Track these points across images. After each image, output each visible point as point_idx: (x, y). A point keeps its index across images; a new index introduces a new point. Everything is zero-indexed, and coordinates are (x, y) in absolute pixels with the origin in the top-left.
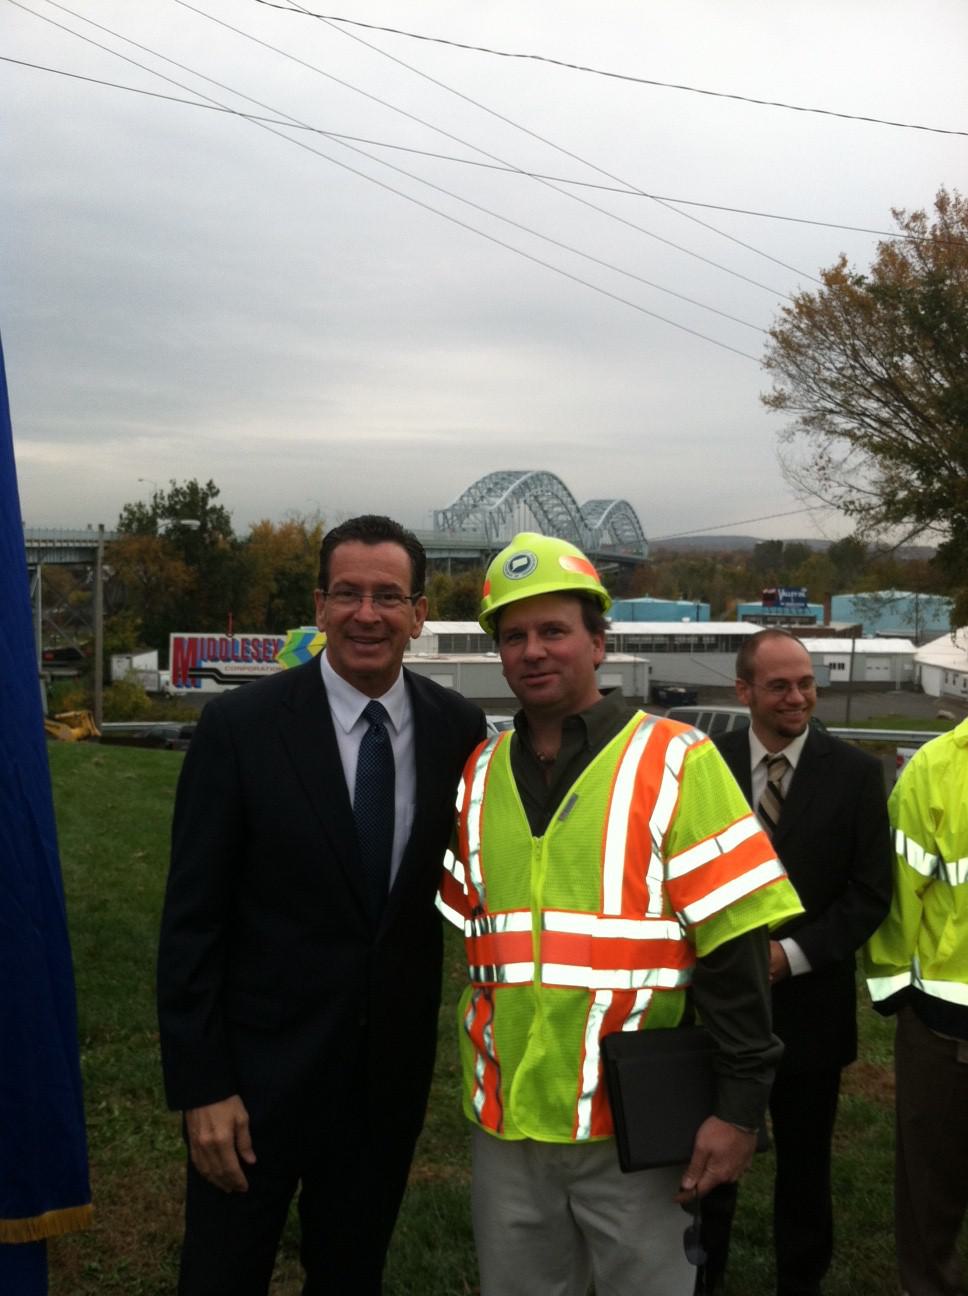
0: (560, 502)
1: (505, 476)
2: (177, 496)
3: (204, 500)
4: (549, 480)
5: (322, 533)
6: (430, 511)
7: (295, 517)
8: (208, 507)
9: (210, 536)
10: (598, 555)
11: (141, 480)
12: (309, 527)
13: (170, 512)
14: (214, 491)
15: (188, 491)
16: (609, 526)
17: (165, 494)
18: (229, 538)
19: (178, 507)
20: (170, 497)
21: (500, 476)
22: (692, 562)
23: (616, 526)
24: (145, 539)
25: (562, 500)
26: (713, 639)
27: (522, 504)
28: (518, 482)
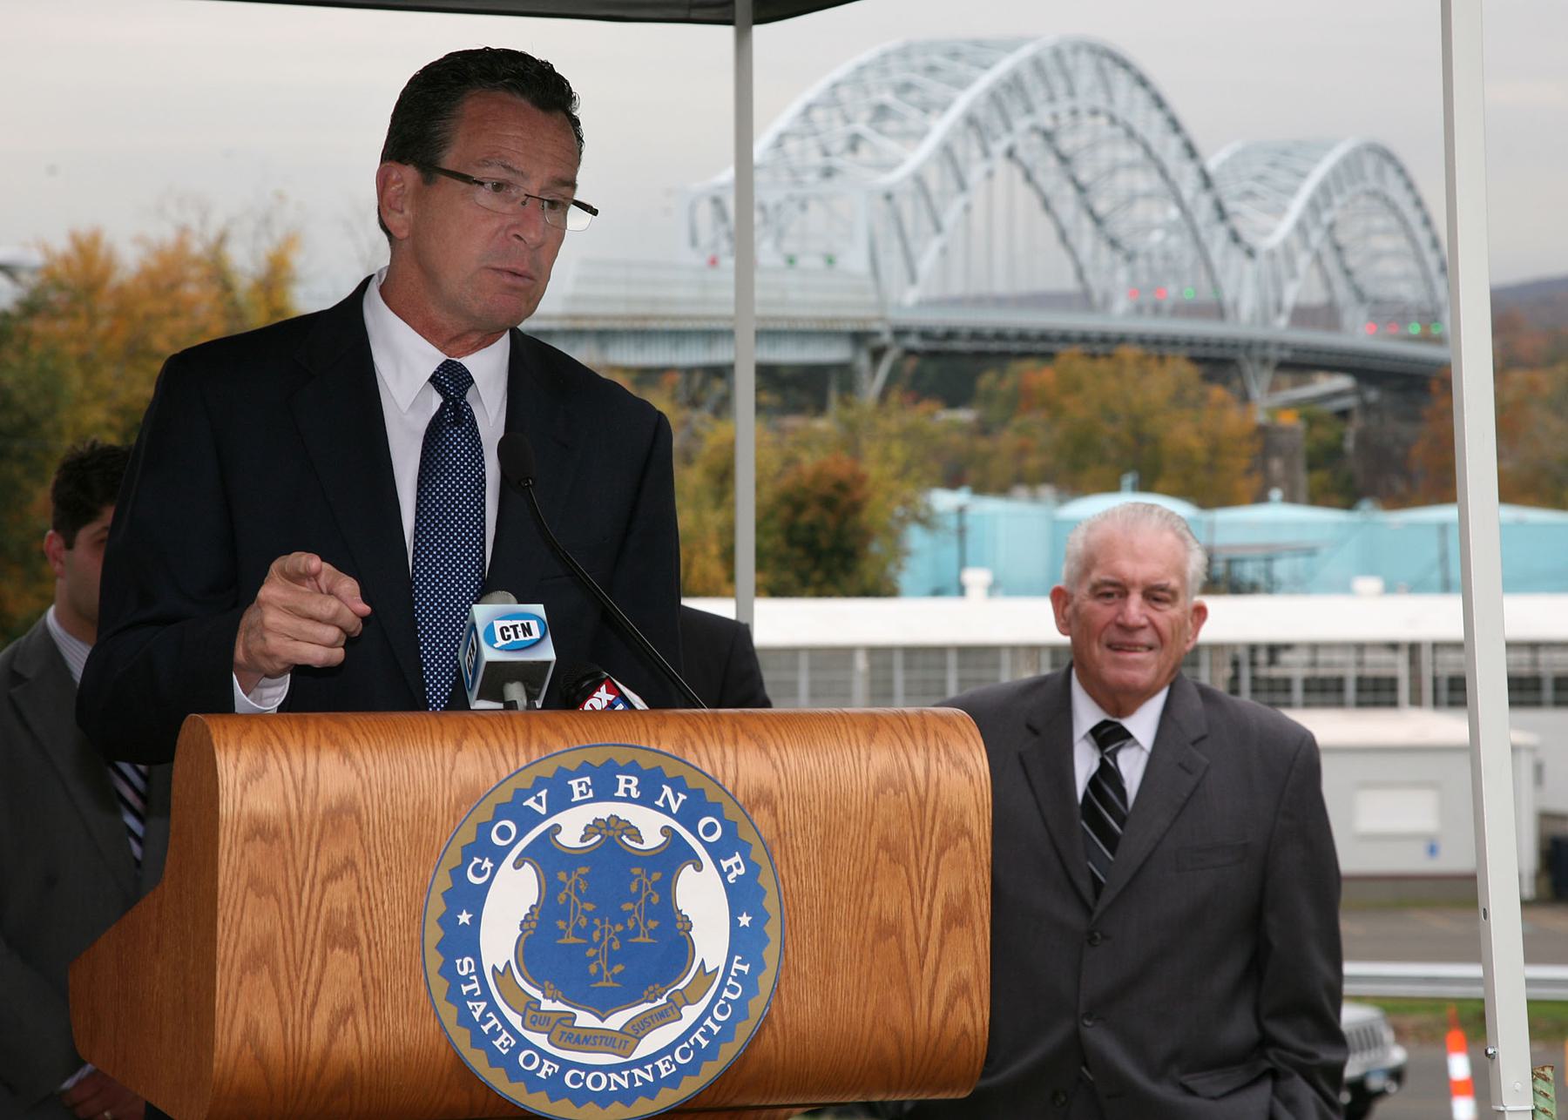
0: (1137, 153)
1: (938, 60)
4: (1100, 70)
6: (135, 351)
10: (1282, 346)
12: (245, 261)
16: (1316, 237)
21: (919, 61)
23: (1343, 237)
25: (1147, 149)
26: (1046, 659)
27: (1000, 165)
28: (985, 81)
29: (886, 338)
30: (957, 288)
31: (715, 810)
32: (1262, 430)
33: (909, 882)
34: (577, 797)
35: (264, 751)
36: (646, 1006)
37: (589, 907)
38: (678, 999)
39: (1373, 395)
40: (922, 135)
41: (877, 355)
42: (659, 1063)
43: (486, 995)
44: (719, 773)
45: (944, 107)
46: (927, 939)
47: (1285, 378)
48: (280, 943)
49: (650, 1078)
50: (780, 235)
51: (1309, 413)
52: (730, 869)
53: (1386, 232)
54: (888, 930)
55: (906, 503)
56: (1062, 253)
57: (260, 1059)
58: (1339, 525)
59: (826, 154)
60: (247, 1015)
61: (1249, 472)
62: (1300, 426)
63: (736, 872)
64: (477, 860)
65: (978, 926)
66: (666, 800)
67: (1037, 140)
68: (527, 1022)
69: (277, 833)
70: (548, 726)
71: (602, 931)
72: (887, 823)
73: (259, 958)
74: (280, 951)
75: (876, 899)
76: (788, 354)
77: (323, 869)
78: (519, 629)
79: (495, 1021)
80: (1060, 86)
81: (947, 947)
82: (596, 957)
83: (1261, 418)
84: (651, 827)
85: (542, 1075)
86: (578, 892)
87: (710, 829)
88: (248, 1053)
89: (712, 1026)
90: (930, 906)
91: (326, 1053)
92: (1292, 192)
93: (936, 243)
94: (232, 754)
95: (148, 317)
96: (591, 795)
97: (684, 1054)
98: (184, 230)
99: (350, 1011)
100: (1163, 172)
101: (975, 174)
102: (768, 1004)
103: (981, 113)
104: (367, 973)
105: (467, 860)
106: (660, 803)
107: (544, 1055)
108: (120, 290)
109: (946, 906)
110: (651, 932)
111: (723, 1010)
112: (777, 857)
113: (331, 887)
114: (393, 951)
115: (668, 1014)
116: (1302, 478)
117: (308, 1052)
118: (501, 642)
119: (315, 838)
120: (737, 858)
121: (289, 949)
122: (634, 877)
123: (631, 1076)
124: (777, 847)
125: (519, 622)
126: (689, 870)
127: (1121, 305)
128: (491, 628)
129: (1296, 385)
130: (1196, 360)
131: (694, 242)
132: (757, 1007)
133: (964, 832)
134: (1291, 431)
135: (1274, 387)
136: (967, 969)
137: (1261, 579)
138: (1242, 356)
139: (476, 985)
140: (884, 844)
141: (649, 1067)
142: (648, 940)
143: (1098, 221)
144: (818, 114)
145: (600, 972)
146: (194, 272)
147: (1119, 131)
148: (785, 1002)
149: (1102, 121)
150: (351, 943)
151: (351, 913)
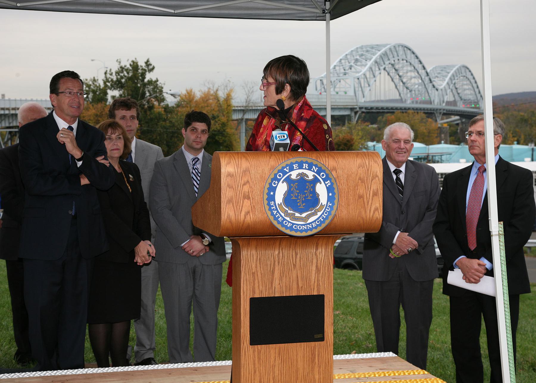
2: (122, 72)
3: (143, 75)
5: (320, 112)
7: (211, 86)
8: (146, 80)
9: (148, 102)
11: (92, 60)
12: (222, 95)
13: (117, 84)
14: (151, 67)
15: (131, 68)
17: (114, 71)
18: (162, 104)
19: (123, 80)
20: (117, 73)
21: (364, 49)
22: (522, 114)
24: (100, 105)
27: (383, 71)
28: (379, 53)
29: (358, 109)
30: (373, 99)
31: (324, 171)
32: (439, 128)
33: (365, 187)
34: (295, 168)
35: (230, 159)
36: (310, 212)
37: (298, 191)
38: (317, 211)
39: (464, 120)
40: (365, 65)
41: (356, 113)
42: (313, 224)
43: (277, 209)
44: (325, 163)
45: (370, 60)
46: (369, 199)
47: (445, 117)
48: (234, 198)
49: (311, 227)
50: (335, 87)
51: (450, 124)
52: (327, 184)
53: (467, 84)
54: (361, 197)
55: (362, 144)
56: (396, 90)
57: (231, 222)
58: (456, 148)
59: (344, 70)
60: (228, 212)
61: (437, 137)
62: (448, 127)
63: (328, 184)
64: (274, 181)
65: (380, 197)
66: (314, 169)
67: (390, 66)
68: (285, 215)
69: (233, 175)
70: (289, 154)
71: (301, 196)
72: (360, 174)
73: (230, 201)
74: (234, 200)
75: (358, 190)
76: (337, 113)
77: (243, 183)
78: (282, 136)
79: (279, 215)
80: (395, 54)
81: (373, 200)
82: (299, 202)
83: (439, 125)
84: (311, 175)
85: (288, 226)
86: (295, 188)
87: (323, 175)
88: (228, 221)
89: (324, 216)
90: (370, 192)
91: (244, 221)
92: (446, 76)
93: (368, 89)
94: (224, 159)
95: (202, 107)
96: (298, 168)
97: (318, 222)
98: (209, 89)
99: (249, 212)
100: (418, 73)
101: (377, 73)
102: (336, 212)
103: (378, 60)
104: (252, 204)
105: (272, 181)
106: (312, 170)
107: (289, 222)
108: (196, 101)
109: (373, 192)
110: (311, 197)
111: (326, 213)
112: (337, 181)
113: (244, 187)
114: (257, 200)
115: (314, 214)
116: (448, 139)
117: (240, 220)
118: (278, 139)
119: (241, 176)
120: (329, 181)
121: (236, 199)
122: (307, 185)
123: (307, 226)
124: (337, 180)
125: (282, 135)
126: (318, 184)
127: (409, 101)
128: (276, 136)
129: (447, 119)
130: (425, 113)
131: (316, 89)
132: (333, 213)
133: (377, 176)
134: (446, 128)
135: (442, 119)
136: (378, 205)
137: (440, 160)
138: (435, 112)
139: (274, 207)
140: (360, 179)
141: (311, 225)
142: (310, 198)
143: (404, 83)
144: (343, 61)
145: (300, 205)
146: (211, 97)
147: (408, 64)
148: (339, 211)
149: (405, 61)
150: (249, 198)
151: (248, 192)
